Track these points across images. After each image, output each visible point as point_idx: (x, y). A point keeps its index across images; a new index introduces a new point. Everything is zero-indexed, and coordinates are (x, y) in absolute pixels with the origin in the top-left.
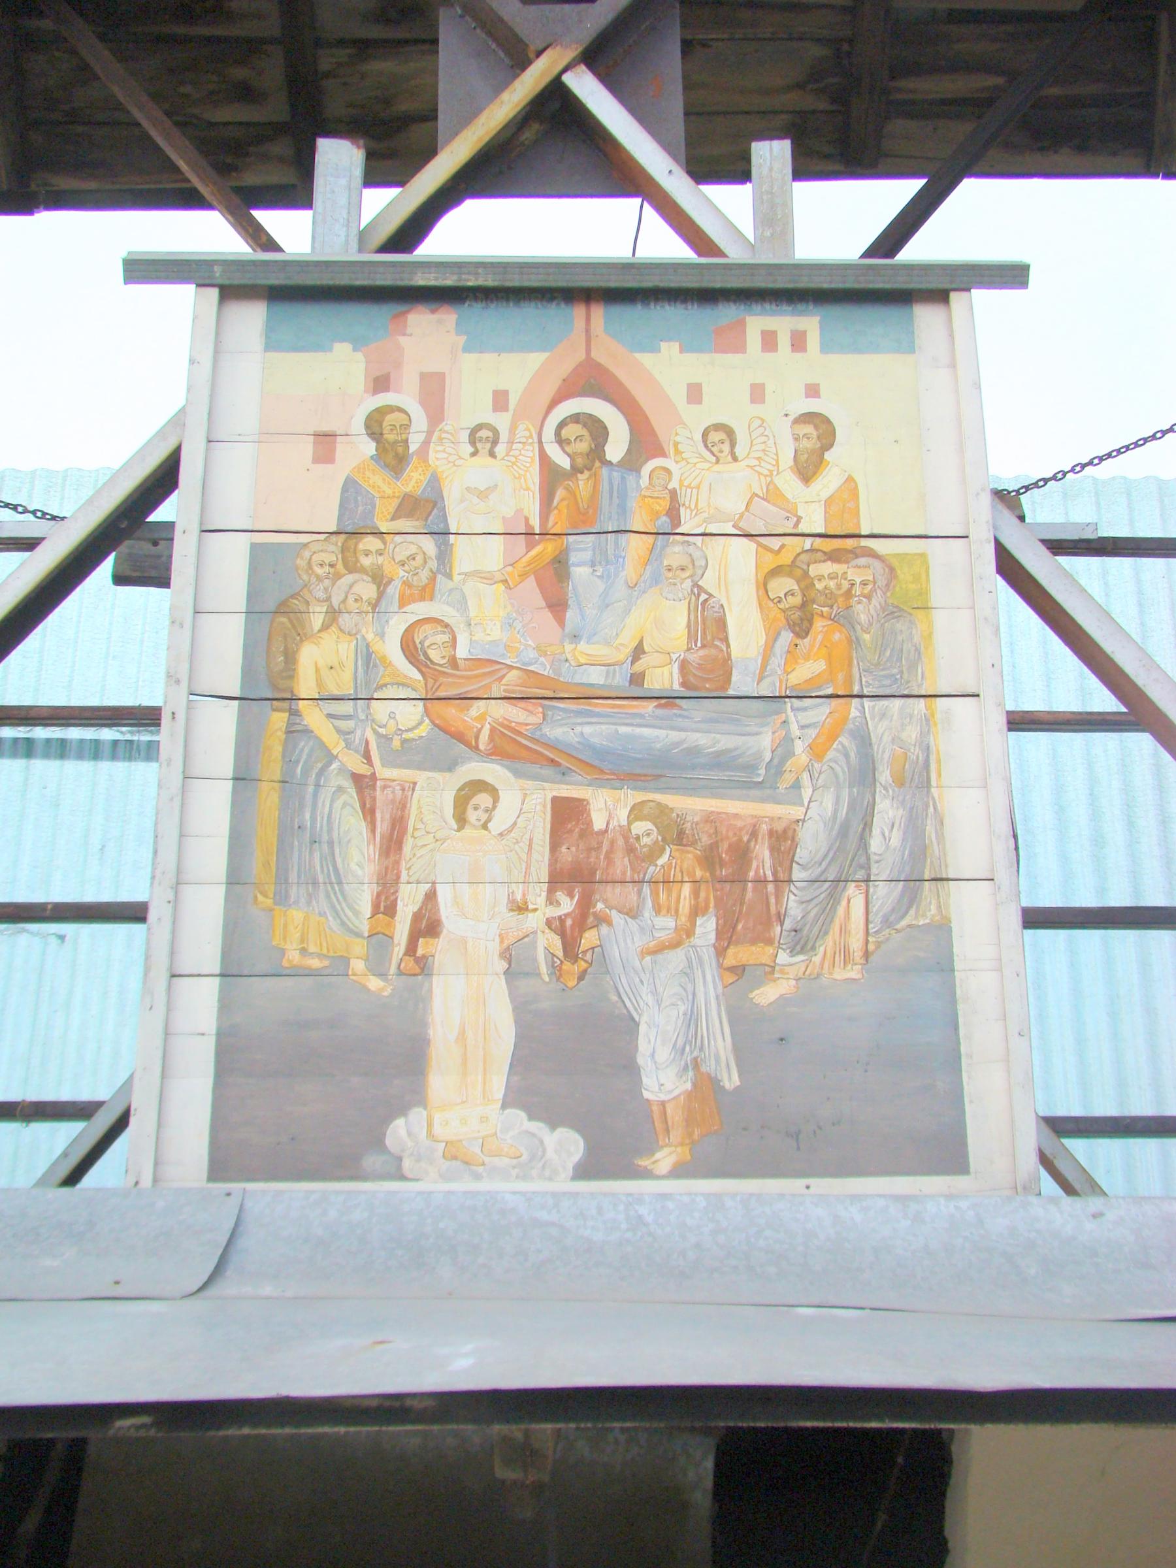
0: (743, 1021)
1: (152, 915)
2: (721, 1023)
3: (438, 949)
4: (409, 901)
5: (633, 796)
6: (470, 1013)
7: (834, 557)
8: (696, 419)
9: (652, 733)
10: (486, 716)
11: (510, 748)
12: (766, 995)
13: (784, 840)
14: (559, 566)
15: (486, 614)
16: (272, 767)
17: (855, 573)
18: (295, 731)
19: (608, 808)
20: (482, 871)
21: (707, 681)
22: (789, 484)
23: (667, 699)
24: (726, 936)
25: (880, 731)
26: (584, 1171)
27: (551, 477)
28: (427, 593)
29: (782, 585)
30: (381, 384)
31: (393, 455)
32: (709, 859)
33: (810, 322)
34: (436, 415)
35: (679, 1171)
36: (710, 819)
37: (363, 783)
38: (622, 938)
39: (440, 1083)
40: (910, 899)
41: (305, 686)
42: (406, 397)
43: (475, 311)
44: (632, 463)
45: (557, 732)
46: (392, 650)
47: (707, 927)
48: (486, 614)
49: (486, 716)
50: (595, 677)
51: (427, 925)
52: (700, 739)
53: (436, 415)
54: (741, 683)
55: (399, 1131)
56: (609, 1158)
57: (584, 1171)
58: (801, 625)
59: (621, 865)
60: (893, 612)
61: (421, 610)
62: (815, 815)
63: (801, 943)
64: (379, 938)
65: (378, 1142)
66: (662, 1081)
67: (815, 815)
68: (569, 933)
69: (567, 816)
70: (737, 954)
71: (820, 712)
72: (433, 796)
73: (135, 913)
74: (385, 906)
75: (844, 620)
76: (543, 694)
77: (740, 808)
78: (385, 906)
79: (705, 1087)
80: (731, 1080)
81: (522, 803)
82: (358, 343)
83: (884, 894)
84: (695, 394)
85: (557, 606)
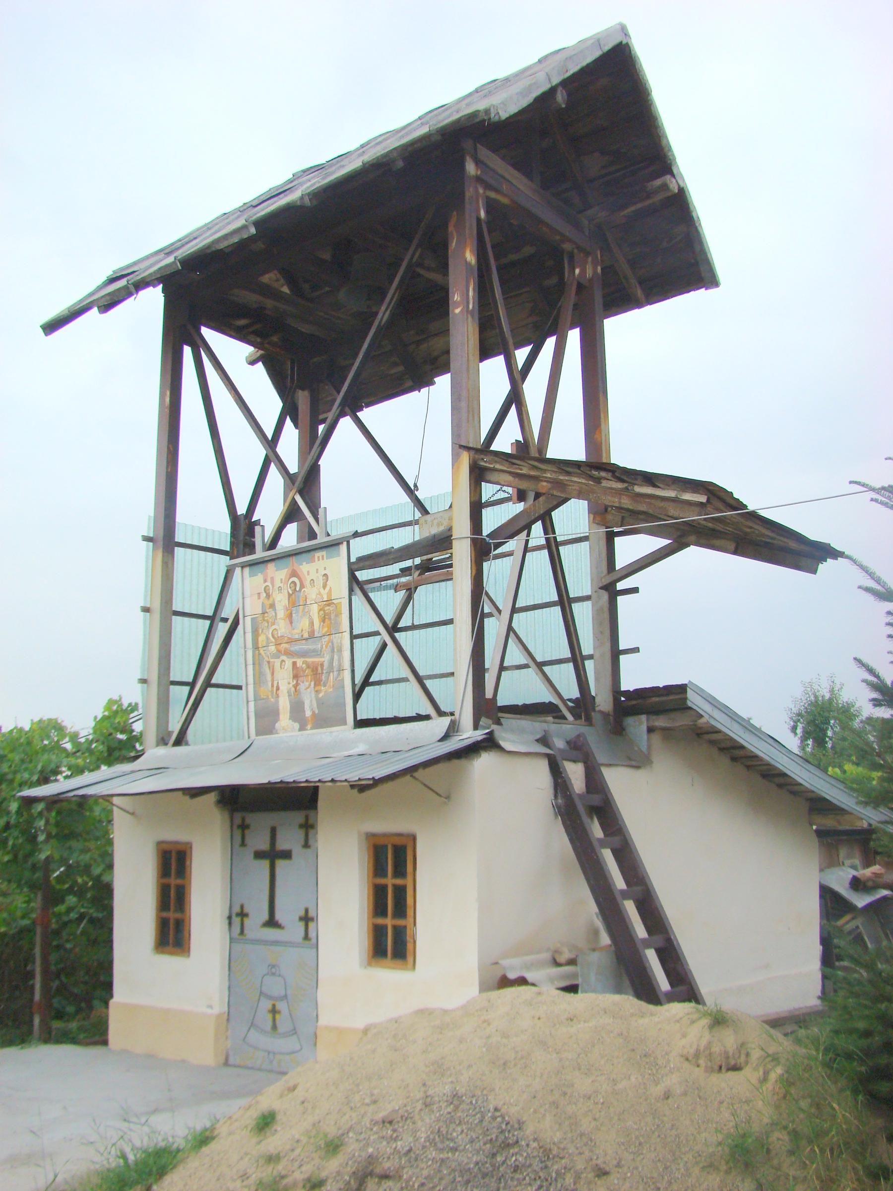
0: (318, 699)
1: (388, 976)
2: (248, 719)
3: (280, 692)
4: (275, 686)
5: (302, 659)
6: (284, 704)
7: (329, 605)
8: (309, 579)
9: (304, 646)
10: (284, 646)
11: (288, 653)
12: (321, 695)
13: (322, 665)
14: (291, 615)
15: (282, 628)
16: (257, 662)
17: (331, 608)
18: (260, 654)
19: (300, 662)
20: (284, 678)
21: (312, 635)
22: (322, 590)
23: (306, 639)
24: (315, 685)
25: (335, 641)
26: (300, 730)
27: (290, 595)
28: (274, 624)
29: (322, 612)
30: (265, 581)
31: (268, 596)
32: (313, 671)
33: (323, 553)
34: (273, 587)
35: (311, 729)
36: (313, 662)
37: (269, 662)
38: (302, 687)
39: (281, 716)
40: (339, 674)
41: (260, 646)
42: (269, 583)
43: (277, 562)
44: (300, 590)
45: (292, 649)
46: (270, 636)
47: (313, 683)
48: (282, 628)
49: (284, 646)
50: (297, 637)
51: (278, 689)
52: (310, 647)
53: (273, 587)
54: (316, 635)
55: (277, 725)
56: (302, 728)
57: (300, 730)
58: (324, 621)
59: (301, 673)
60: (337, 616)
61: (274, 627)
62: (326, 659)
63: (325, 686)
64: (272, 691)
65: (274, 727)
66: (308, 713)
67: (326, 659)
68: (296, 686)
69: (294, 664)
70: (317, 688)
71: (327, 638)
72: (277, 663)
73: (239, 688)
74: (273, 686)
75: (330, 619)
76: (291, 641)
77: (316, 660)
78: (273, 686)
79: (314, 713)
80: (317, 712)
81: (288, 663)
82: (261, 572)
83: (336, 673)
84: (308, 572)
85: (291, 623)
